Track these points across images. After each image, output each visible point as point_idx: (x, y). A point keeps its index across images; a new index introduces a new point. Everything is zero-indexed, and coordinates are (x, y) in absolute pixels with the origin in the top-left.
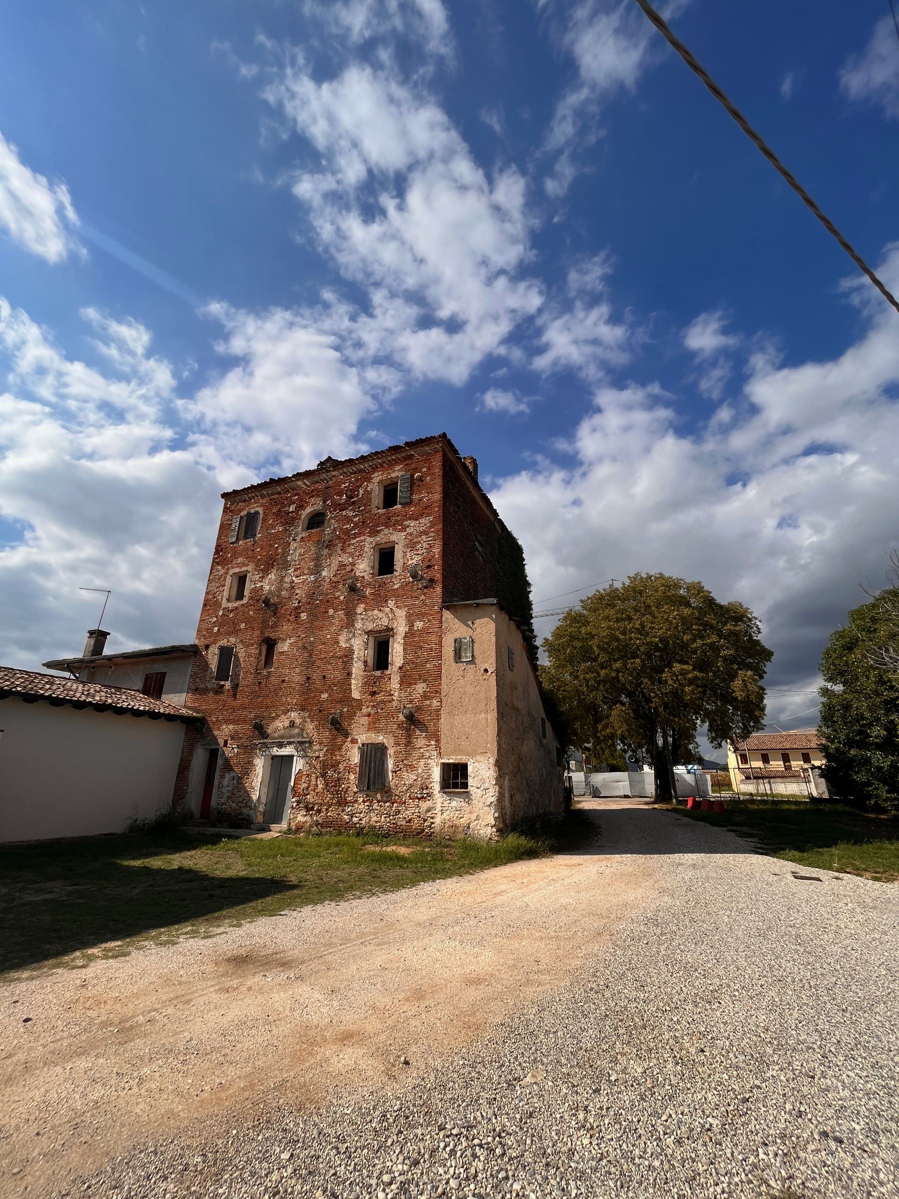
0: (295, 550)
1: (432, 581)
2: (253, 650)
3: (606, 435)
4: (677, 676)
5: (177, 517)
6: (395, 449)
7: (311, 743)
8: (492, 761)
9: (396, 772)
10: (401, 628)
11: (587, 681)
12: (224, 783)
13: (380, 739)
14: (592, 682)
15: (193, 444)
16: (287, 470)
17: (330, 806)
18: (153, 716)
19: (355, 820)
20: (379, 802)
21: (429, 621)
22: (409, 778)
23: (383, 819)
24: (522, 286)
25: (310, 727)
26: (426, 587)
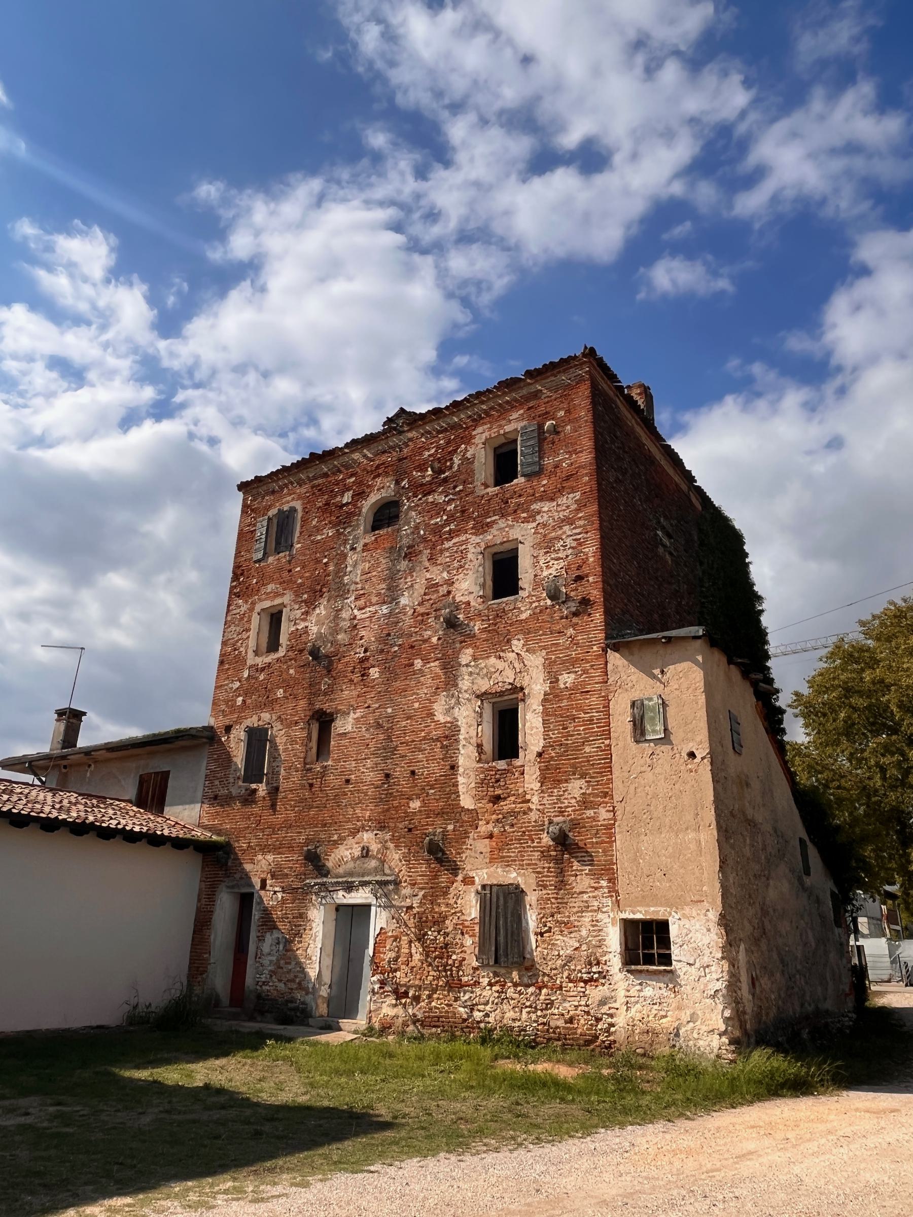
0: (355, 565)
1: (585, 602)
2: (298, 732)
3: (881, 313)
5: (164, 524)
6: (510, 384)
7: (397, 883)
8: (713, 916)
9: (542, 934)
10: (537, 686)
11: (883, 770)
12: (263, 947)
13: (512, 876)
14: (893, 772)
15: (183, 406)
16: (333, 437)
17: (434, 991)
18: (154, 840)
19: (478, 1015)
20: (515, 985)
21: (585, 672)
22: (566, 944)
23: (524, 1015)
24: (709, 78)
25: (395, 857)
26: (576, 614)
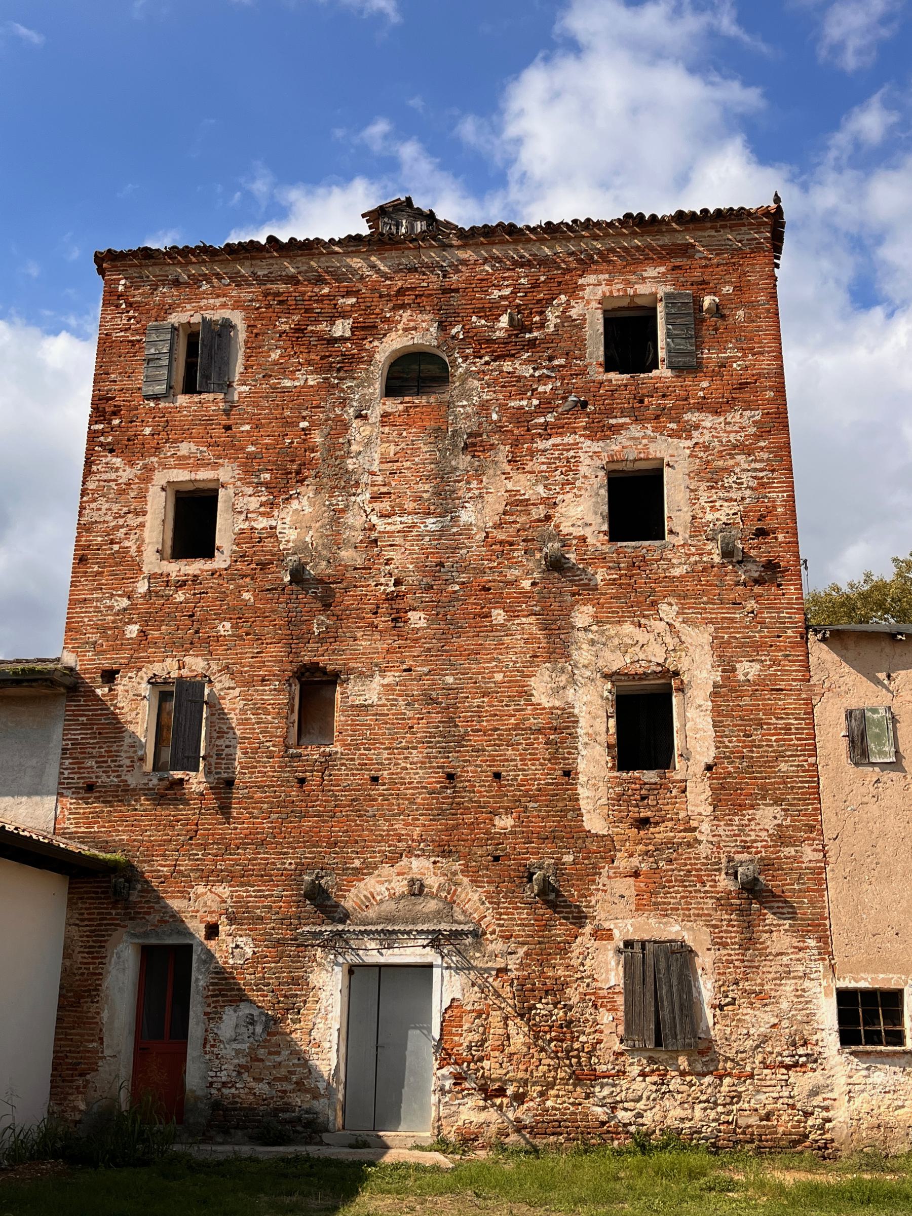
7: (478, 935)
9: (721, 1007)
10: (700, 673)
13: (673, 930)
17: (551, 1086)
19: (623, 1116)
20: (683, 1074)
21: (775, 662)
22: (759, 1020)
26: (758, 581)
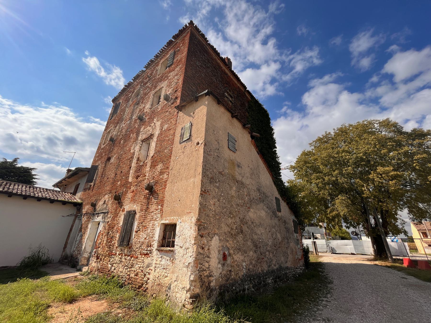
4: (381, 175)
8: (194, 220)
14: (320, 185)
